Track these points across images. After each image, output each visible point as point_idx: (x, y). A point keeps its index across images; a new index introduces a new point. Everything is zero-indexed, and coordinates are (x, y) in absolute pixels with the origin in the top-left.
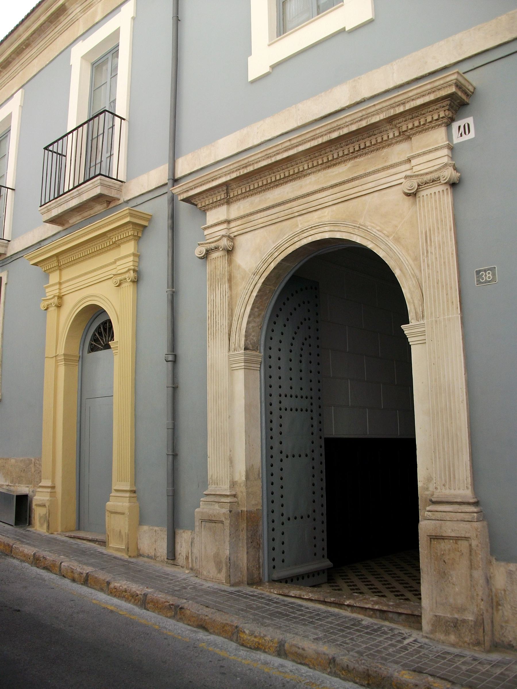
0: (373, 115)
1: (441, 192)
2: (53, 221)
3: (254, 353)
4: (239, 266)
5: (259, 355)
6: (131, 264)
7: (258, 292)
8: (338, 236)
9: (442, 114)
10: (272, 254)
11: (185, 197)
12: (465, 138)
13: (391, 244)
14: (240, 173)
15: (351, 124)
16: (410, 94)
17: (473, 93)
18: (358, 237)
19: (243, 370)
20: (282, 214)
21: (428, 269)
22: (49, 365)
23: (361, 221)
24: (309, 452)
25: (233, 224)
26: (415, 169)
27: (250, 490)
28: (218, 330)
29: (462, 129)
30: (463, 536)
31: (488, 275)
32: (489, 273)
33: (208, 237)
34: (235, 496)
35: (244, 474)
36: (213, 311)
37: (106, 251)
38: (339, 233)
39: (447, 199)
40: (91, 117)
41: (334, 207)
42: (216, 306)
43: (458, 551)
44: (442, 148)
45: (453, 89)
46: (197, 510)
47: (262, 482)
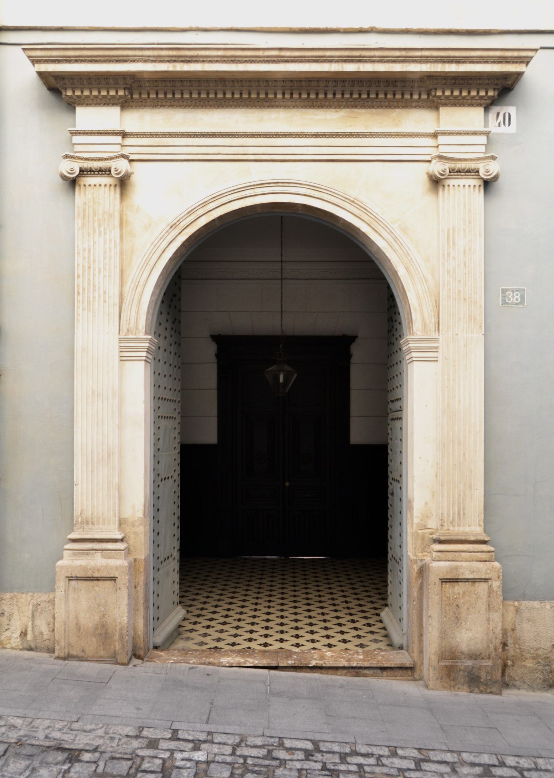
10: (205, 204)
12: (504, 129)
19: (143, 363)
26: (442, 149)
29: (501, 118)
30: (483, 577)
33: (78, 148)
43: (475, 594)
46: (60, 563)
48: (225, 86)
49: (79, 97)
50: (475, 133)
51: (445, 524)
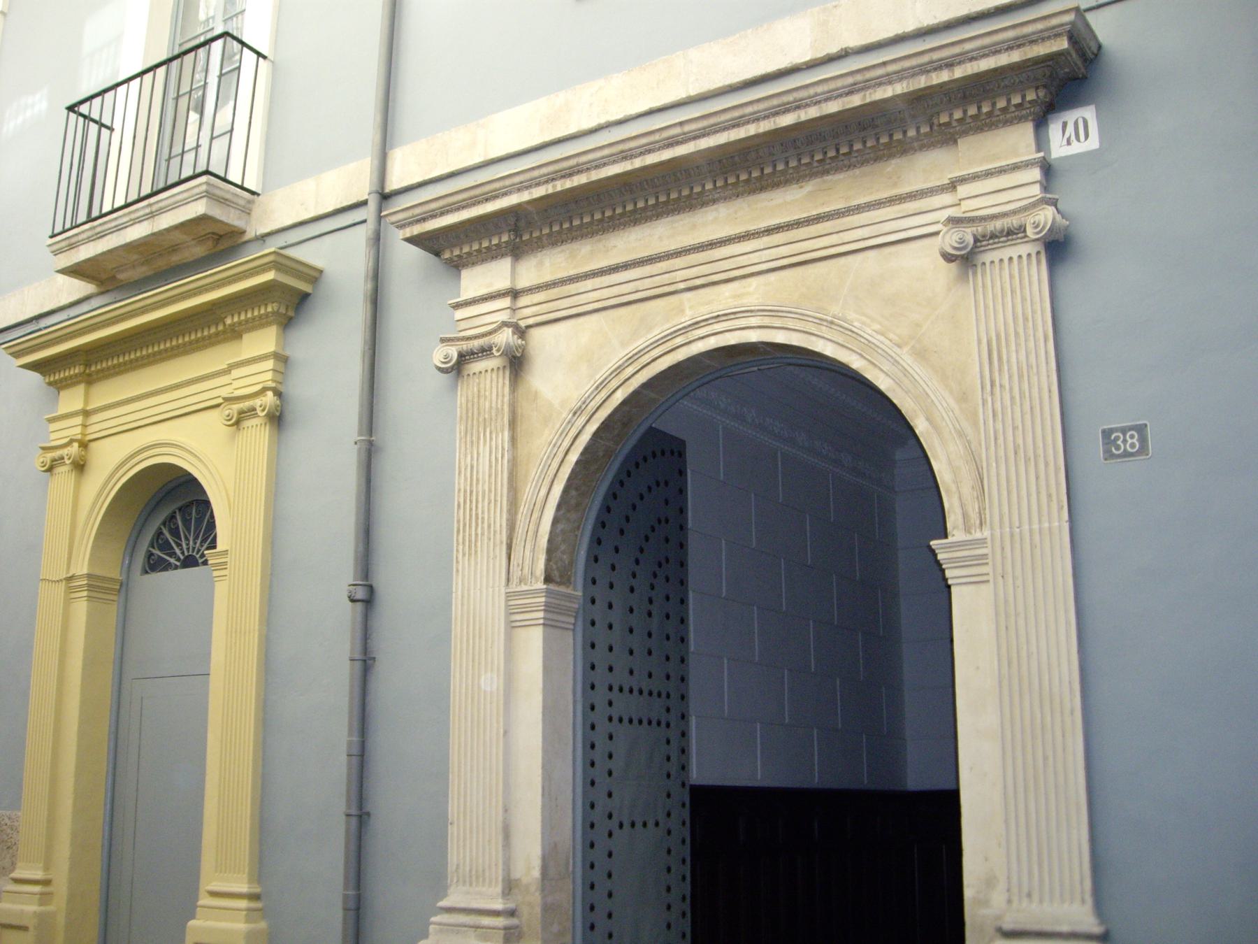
0: (880, 84)
1: (1025, 258)
2: (75, 271)
3: (562, 589)
4: (536, 395)
5: (577, 591)
6: (269, 376)
7: (582, 454)
8: (780, 338)
9: (1031, 96)
10: (619, 370)
11: (415, 233)
13: (907, 360)
14: (554, 187)
15: (826, 100)
16: (968, 46)
17: (1096, 55)
18: (829, 344)
19: (540, 629)
20: (648, 283)
21: (994, 421)
22: (50, 598)
23: (835, 309)
24: (661, 817)
25: (523, 301)
27: (550, 899)
28: (483, 534)
29: (1070, 129)
31: (1130, 441)
32: (1132, 437)
34: (512, 913)
35: (537, 864)
36: (471, 492)
37: (205, 347)
38: (782, 332)
39: (1038, 273)
40: (176, 52)
41: (772, 277)
42: (478, 480)
44: (1027, 165)
45: (1063, 44)
47: (574, 882)
48: (632, 192)
49: (459, 256)
50: (1015, 167)
51: (1015, 899)
